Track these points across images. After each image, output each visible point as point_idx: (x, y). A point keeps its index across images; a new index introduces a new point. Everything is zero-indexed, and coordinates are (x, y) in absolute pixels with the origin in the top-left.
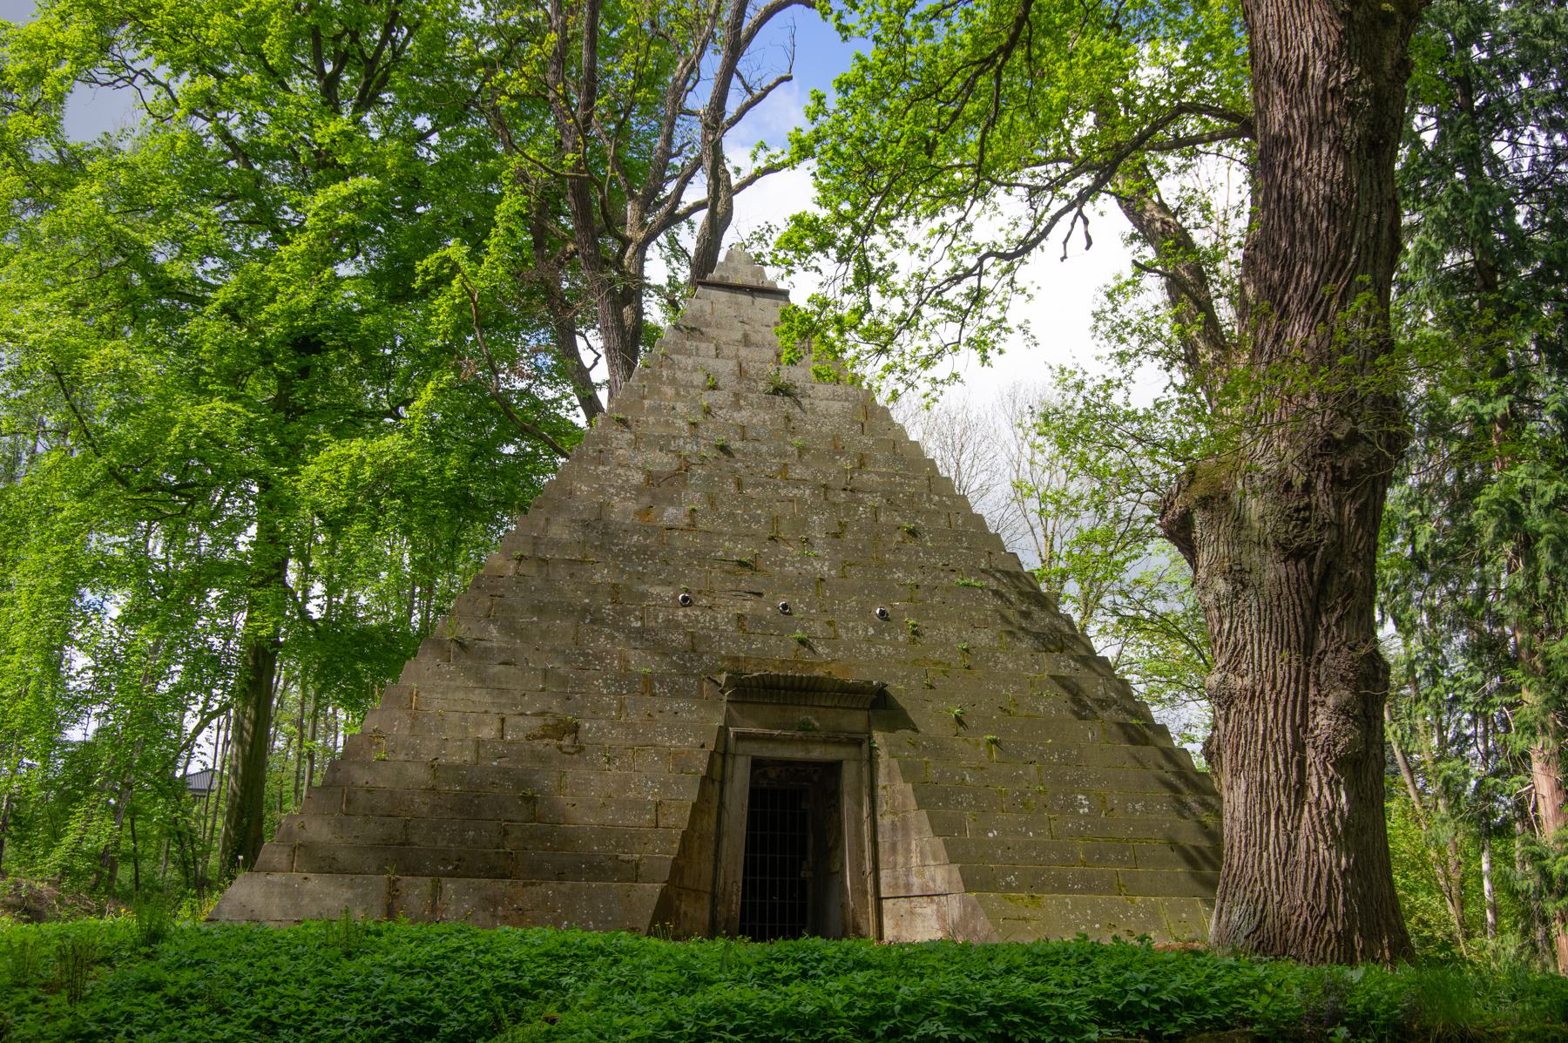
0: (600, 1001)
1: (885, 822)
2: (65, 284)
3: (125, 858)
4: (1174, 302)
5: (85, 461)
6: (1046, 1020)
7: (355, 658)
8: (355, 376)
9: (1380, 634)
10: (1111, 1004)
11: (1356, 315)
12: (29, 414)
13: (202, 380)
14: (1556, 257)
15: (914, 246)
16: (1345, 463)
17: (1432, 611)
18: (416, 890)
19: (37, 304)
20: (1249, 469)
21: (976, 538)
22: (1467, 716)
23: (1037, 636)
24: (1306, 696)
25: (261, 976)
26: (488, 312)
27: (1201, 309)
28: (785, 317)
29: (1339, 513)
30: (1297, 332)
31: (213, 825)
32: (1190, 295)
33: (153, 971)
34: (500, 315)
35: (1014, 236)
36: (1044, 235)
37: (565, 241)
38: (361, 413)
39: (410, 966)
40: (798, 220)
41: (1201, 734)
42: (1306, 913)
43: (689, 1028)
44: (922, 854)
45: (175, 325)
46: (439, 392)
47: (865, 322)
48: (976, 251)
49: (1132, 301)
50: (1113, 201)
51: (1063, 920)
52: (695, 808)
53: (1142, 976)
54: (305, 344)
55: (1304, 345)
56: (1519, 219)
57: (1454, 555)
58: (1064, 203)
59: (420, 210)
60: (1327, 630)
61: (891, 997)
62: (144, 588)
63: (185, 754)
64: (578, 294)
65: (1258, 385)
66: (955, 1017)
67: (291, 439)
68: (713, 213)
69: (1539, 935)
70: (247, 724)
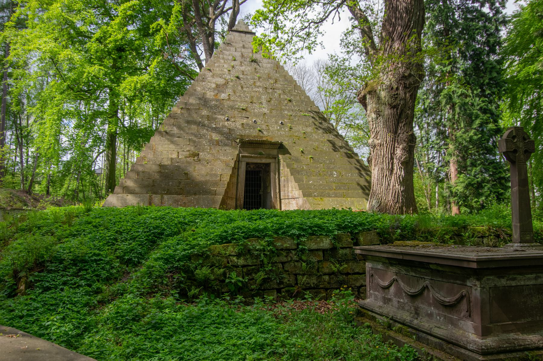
0: (206, 225)
1: (282, 179)
2: (52, 33)
3: (81, 191)
4: (363, 37)
5: (61, 84)
6: (324, 229)
7: (138, 137)
8: (134, 58)
9: (414, 129)
10: (341, 225)
11: (412, 41)
12: (45, 71)
13: (92, 60)
14: (465, 27)
15: (291, 20)
16: (407, 82)
17: (428, 124)
18: (156, 199)
19: (45, 39)
20: (382, 83)
21: (309, 102)
22: (435, 151)
23: (324, 129)
24: (394, 145)
25: (117, 220)
26: (171, 40)
27: (370, 39)
28: (255, 40)
29: (405, 96)
30: (396, 45)
31: (102, 182)
32: (367, 35)
33: (89, 219)
34: (175, 40)
35: (319, 17)
36: (327, 17)
37: (192, 19)
38: (136, 69)
39: (156, 217)
40: (258, 12)
41: (367, 156)
42: (392, 202)
43: (230, 232)
44: (292, 187)
45: (83, 44)
46: (158, 63)
47: (277, 41)
48: (308, 21)
49: (351, 36)
50: (347, 8)
51: (328, 204)
52: (231, 176)
53: (349, 218)
54: (120, 49)
55: (398, 49)
56: (456, 16)
57: (435, 108)
58: (333, 8)
59: (151, 10)
60: (401, 128)
61: (283, 224)
62: (80, 119)
63: (94, 164)
64: (196, 34)
65: (385, 60)
66: (300, 229)
67: (117, 77)
68: (234, 10)
69: (448, 207)
70: (110, 155)
